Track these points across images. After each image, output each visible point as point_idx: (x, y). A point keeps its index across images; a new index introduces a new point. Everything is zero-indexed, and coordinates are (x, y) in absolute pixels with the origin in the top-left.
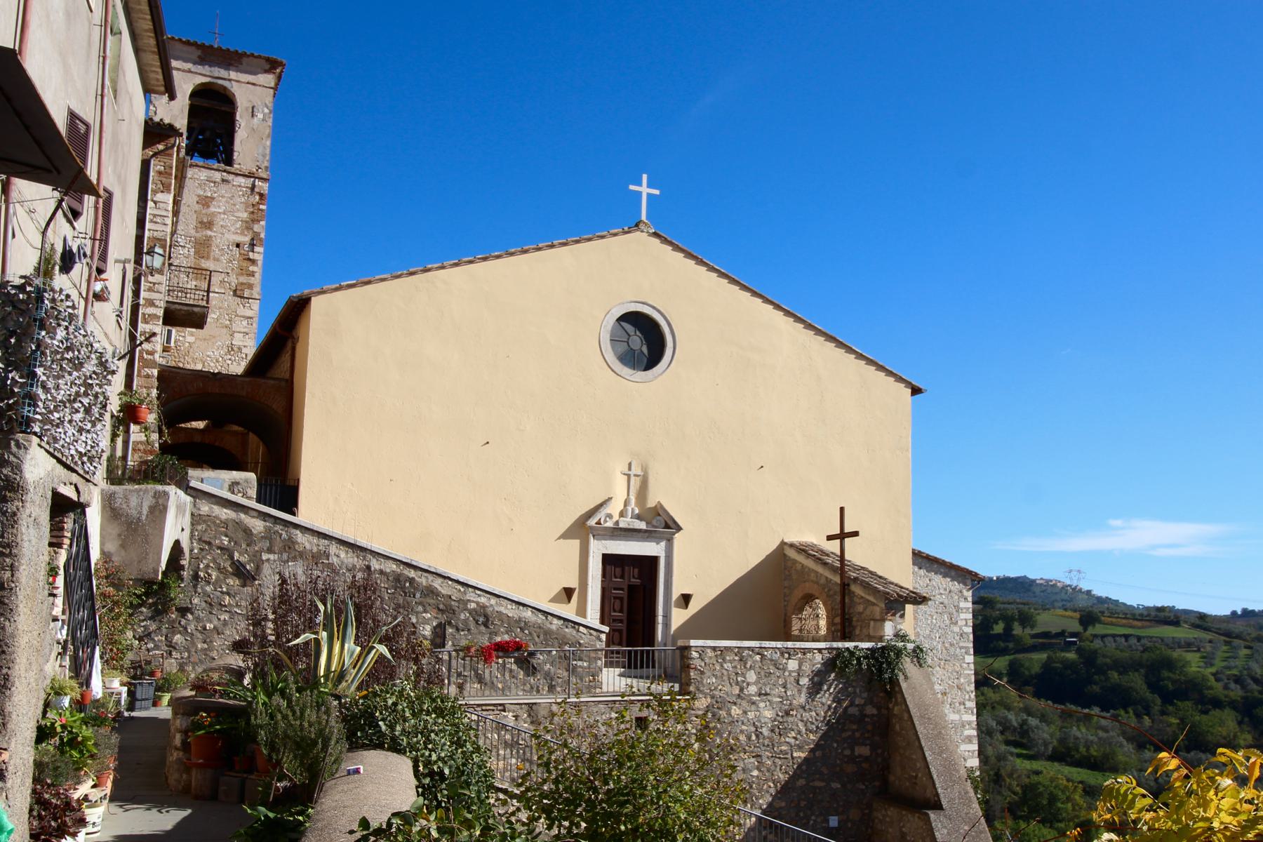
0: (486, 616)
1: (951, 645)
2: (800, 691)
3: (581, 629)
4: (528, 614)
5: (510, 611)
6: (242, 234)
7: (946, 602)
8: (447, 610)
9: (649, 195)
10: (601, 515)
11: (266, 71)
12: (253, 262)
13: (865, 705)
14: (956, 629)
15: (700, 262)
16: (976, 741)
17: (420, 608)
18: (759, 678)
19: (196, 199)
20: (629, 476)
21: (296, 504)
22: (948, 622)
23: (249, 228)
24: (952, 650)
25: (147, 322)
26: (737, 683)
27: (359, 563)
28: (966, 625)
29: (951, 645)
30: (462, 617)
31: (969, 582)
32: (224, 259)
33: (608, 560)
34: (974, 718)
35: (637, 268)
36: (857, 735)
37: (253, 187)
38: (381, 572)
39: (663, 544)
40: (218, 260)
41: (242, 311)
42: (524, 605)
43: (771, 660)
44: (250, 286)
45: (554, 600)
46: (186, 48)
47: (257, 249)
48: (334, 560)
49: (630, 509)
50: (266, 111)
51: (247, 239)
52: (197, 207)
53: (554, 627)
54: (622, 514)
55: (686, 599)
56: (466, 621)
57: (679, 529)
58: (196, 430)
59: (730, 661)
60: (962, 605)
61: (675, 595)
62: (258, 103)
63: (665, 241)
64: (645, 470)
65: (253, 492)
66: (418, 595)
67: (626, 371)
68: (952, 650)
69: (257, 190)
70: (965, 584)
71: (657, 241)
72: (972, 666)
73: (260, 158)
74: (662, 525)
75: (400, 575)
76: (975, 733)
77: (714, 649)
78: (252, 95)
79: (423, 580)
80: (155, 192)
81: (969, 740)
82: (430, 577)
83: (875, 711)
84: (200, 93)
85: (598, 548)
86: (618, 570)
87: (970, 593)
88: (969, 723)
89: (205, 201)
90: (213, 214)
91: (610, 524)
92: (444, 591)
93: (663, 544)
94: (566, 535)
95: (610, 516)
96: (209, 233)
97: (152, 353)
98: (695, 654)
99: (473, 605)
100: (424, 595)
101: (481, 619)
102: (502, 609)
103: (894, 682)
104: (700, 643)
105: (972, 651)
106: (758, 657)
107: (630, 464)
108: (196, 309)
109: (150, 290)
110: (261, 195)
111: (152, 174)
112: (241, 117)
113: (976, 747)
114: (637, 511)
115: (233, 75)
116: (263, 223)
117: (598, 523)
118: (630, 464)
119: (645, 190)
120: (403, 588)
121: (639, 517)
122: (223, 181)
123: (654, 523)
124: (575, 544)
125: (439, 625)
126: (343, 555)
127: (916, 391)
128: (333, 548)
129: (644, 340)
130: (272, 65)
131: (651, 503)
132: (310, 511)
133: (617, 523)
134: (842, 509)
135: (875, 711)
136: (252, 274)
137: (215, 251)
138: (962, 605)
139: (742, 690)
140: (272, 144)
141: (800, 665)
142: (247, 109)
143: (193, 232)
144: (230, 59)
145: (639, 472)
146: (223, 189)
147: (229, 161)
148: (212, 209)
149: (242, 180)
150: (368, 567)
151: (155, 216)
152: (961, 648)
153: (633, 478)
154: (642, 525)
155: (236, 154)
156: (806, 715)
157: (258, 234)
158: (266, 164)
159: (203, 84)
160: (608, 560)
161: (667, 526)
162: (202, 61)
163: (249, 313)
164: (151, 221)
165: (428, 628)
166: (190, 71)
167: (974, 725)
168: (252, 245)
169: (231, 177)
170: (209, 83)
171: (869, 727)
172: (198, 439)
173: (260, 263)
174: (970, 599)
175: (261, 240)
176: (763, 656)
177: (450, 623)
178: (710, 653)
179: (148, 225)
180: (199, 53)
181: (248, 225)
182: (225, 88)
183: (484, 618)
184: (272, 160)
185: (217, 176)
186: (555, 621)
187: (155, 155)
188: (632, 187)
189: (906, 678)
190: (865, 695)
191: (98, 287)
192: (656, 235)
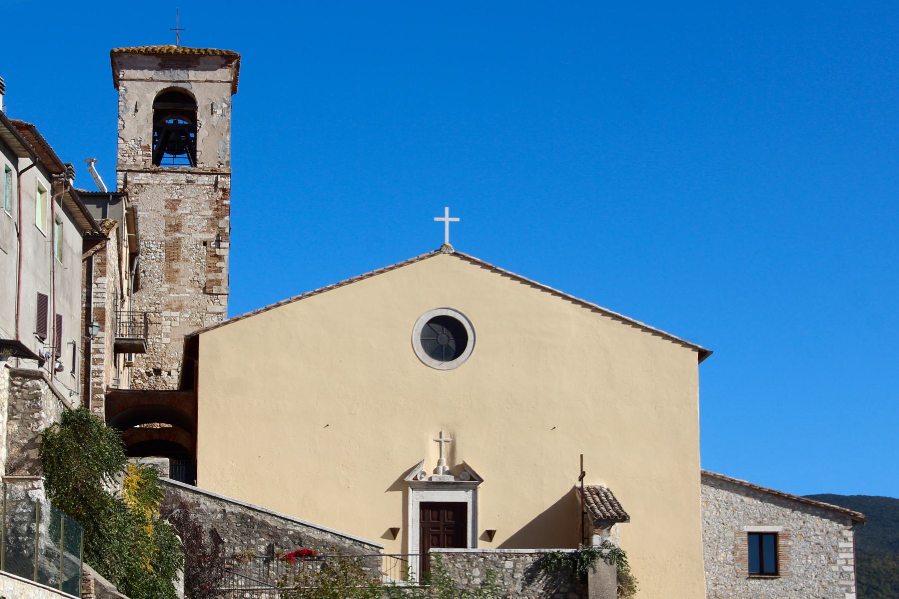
0: (300, 539)
1: (829, 583)
2: (515, 583)
3: (366, 546)
5: (316, 535)
6: (208, 231)
7: (823, 543)
8: (275, 535)
10: (417, 472)
11: (222, 66)
12: (220, 258)
13: (568, 592)
14: (835, 568)
15: (494, 270)
17: (258, 535)
19: (164, 204)
20: (440, 442)
21: (195, 476)
22: (825, 562)
23: (214, 225)
26: (466, 576)
27: (219, 509)
28: (847, 564)
29: (829, 583)
30: (285, 540)
31: (850, 522)
32: (192, 259)
33: (424, 506)
35: (443, 283)
37: (217, 182)
38: (232, 513)
39: (470, 492)
40: (187, 260)
41: (213, 308)
42: (325, 531)
43: (492, 561)
45: (385, 536)
46: (146, 59)
47: (223, 245)
48: (202, 506)
49: (441, 467)
50: (225, 106)
51: (213, 236)
52: (166, 212)
53: (346, 545)
54: (436, 471)
55: (490, 535)
56: (287, 542)
57: (481, 481)
58: (167, 423)
59: (460, 562)
60: (842, 545)
61: (480, 532)
62: (217, 100)
63: (464, 258)
64: (453, 437)
65: (167, 471)
66: (256, 527)
67: (435, 363)
69: (220, 186)
71: (457, 259)
73: (222, 153)
74: (467, 478)
75: (244, 515)
77: (448, 554)
78: (209, 89)
79: (259, 517)
80: (96, 277)
84: (163, 98)
85: (416, 498)
86: (435, 513)
87: (851, 534)
89: (172, 205)
90: (181, 217)
91: (425, 479)
93: (470, 492)
94: (393, 488)
95: (424, 473)
96: (178, 235)
97: (99, 384)
98: (433, 558)
99: (291, 532)
100: (260, 527)
101: (297, 541)
102: (311, 534)
104: (437, 550)
105: (853, 589)
107: (441, 433)
108: (136, 342)
109: (97, 342)
110: (224, 190)
111: (94, 265)
114: (447, 468)
115: (192, 74)
116: (227, 218)
117: (415, 479)
118: (441, 433)
119: (447, 220)
120: (246, 523)
121: (449, 473)
122: (188, 182)
123: (461, 477)
124: (399, 494)
125: (270, 545)
126: (208, 504)
127: (703, 355)
128: (202, 500)
129: (447, 338)
130: (227, 59)
131: (458, 462)
134: (582, 456)
136: (220, 270)
137: (185, 253)
138: (842, 545)
139: (469, 581)
140: (232, 138)
141: (515, 565)
142: (206, 107)
143: (163, 236)
145: (449, 439)
146: (189, 190)
147: (194, 161)
148: (180, 211)
149: (205, 179)
150: (224, 511)
151: (97, 293)
152: (843, 586)
153: (443, 444)
154: (451, 479)
155: (198, 154)
157: (222, 230)
158: (227, 159)
159: (164, 90)
160: (424, 506)
161: (472, 479)
162: (162, 67)
163: (219, 309)
164: (95, 297)
165: (263, 547)
166: (152, 80)
168: (218, 241)
169: (195, 177)
170: (170, 88)
172: (156, 436)
173: (226, 258)
174: (851, 539)
175: (226, 235)
176: (485, 558)
177: (277, 544)
179: (93, 300)
180: (159, 61)
181: (213, 222)
182: (185, 90)
184: (232, 155)
185: (182, 178)
186: (348, 541)
187: (95, 252)
188: (437, 219)
189: (595, 571)
190: (568, 585)
191: (57, 366)
192: (455, 254)
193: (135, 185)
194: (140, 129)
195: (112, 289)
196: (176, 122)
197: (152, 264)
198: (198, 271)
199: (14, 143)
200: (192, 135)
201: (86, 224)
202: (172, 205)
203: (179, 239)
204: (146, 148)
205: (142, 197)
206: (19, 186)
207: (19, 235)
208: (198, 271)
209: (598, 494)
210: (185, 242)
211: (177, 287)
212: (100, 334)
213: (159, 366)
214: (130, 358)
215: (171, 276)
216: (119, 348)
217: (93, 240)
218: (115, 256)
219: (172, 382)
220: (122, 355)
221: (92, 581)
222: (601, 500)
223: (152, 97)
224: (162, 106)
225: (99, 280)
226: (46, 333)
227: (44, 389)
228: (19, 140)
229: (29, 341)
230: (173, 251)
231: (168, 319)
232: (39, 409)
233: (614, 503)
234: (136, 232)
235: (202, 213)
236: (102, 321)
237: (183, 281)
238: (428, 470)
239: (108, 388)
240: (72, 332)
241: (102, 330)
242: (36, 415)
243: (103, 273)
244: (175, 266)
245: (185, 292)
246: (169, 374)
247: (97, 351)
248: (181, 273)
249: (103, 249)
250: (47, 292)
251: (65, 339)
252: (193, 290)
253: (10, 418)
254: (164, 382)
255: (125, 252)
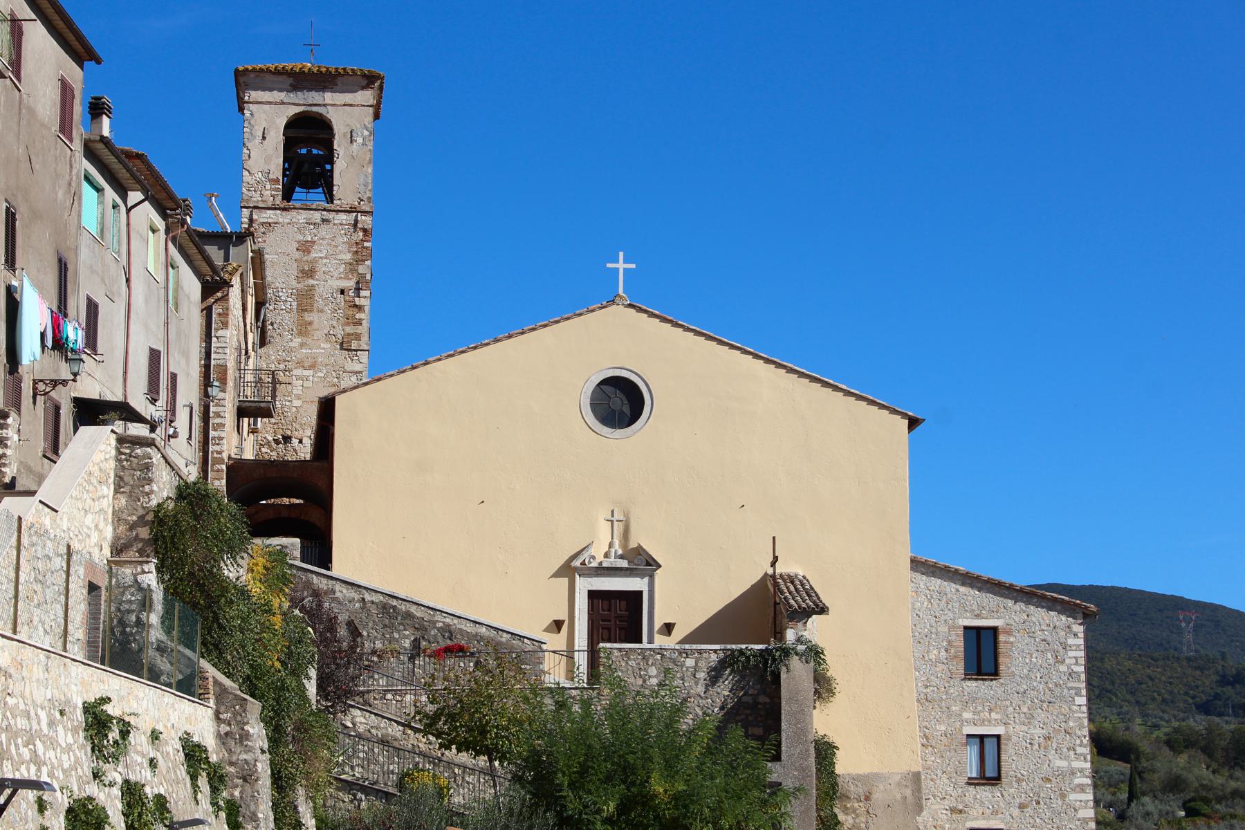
2: (697, 683)
4: (483, 630)
5: (469, 628)
6: (346, 278)
7: (1049, 639)
8: (421, 627)
9: (625, 269)
10: (585, 556)
11: (363, 88)
12: (360, 308)
14: (1063, 668)
15: (675, 324)
16: (1090, 790)
18: (659, 673)
19: (295, 245)
22: (1051, 661)
23: (354, 271)
24: (1058, 691)
25: (215, 430)
26: (640, 676)
28: (1076, 663)
33: (593, 595)
34: (1088, 765)
36: (750, 718)
37: (356, 221)
38: (373, 602)
39: (646, 579)
40: (322, 311)
41: (350, 366)
44: (358, 337)
45: (547, 630)
46: (276, 78)
47: (363, 293)
48: (338, 594)
50: (366, 133)
51: (351, 283)
52: (297, 255)
54: (606, 555)
55: (668, 628)
60: (1071, 641)
61: (658, 625)
62: (357, 126)
64: (627, 515)
65: (297, 554)
68: (1058, 691)
69: (360, 226)
70: (1074, 618)
71: (633, 311)
72: (1084, 709)
73: (362, 188)
74: (643, 563)
76: (1089, 781)
77: (620, 650)
78: (348, 114)
79: (403, 607)
80: (217, 330)
81: (1082, 788)
82: (408, 605)
83: (768, 700)
85: (584, 585)
87: (1081, 628)
88: (1082, 770)
89: (305, 247)
90: (315, 260)
91: (594, 564)
92: (419, 614)
93: (646, 579)
94: (557, 574)
95: (594, 557)
96: (311, 282)
97: (220, 453)
99: (440, 625)
100: (404, 618)
102: (463, 627)
103: (777, 677)
104: (608, 645)
105: (1084, 692)
106: (659, 657)
108: (262, 405)
109: (217, 405)
110: (365, 230)
112: (339, 145)
113: (1091, 797)
114: (620, 552)
115: (329, 97)
116: (368, 263)
117: (583, 563)
119: (621, 266)
120: (388, 613)
121: (622, 557)
122: (323, 220)
125: (415, 639)
127: (913, 423)
128: (338, 587)
130: (370, 80)
131: (633, 545)
132: (342, 565)
133: (601, 563)
135: (768, 700)
137: (319, 303)
138: (1071, 641)
139: (644, 681)
140: (374, 170)
142: (345, 135)
144: (323, 80)
146: (324, 231)
147: (330, 198)
148: (313, 255)
149: (343, 217)
150: (363, 599)
152: (1070, 689)
153: (616, 524)
155: (335, 188)
156: (703, 702)
158: (369, 194)
160: (593, 595)
161: (648, 564)
162: (295, 88)
163: (358, 367)
165: (408, 641)
167: (1087, 773)
168: (358, 289)
169: (331, 216)
171: (762, 713)
172: (285, 514)
173: (367, 308)
174: (1081, 635)
175: (366, 282)
178: (616, 653)
179: (213, 356)
180: (291, 80)
181: (352, 267)
182: (321, 115)
183: (448, 631)
185: (317, 216)
186: (505, 635)
187: (216, 301)
189: (788, 671)
191: (171, 431)
192: (631, 306)
193: (263, 224)
194: (268, 160)
195: (235, 344)
196: (309, 152)
197: (281, 315)
198: (335, 323)
199: (123, 174)
200: (328, 167)
201: (205, 268)
202: (305, 247)
203: (313, 286)
204: (276, 181)
205: (270, 238)
206: (128, 225)
207: (128, 280)
208: (335, 323)
209: (792, 582)
210: (319, 290)
211: (309, 341)
212: (221, 395)
213: (289, 433)
214: (255, 424)
215: (304, 329)
216: (242, 412)
217: (213, 287)
218: (239, 305)
219: (304, 451)
220: (246, 420)
221: (211, 680)
222: (796, 589)
223: (282, 122)
224: (292, 134)
225: (220, 333)
226: (158, 393)
227: (156, 458)
228: (128, 170)
229: (139, 403)
230: (305, 301)
231: (299, 378)
232: (150, 481)
233: (811, 592)
234: (263, 278)
235: (339, 257)
236: (223, 380)
237: (317, 335)
238: (598, 553)
239: (230, 458)
240: (189, 392)
241: (224, 391)
242: (147, 488)
243: (225, 325)
244: (308, 317)
245: (319, 347)
246: (301, 442)
247: (218, 415)
248: (315, 326)
249: (225, 298)
250: (160, 347)
251: (181, 400)
252: (328, 345)
253: (116, 492)
254: (295, 451)
255: (251, 301)
